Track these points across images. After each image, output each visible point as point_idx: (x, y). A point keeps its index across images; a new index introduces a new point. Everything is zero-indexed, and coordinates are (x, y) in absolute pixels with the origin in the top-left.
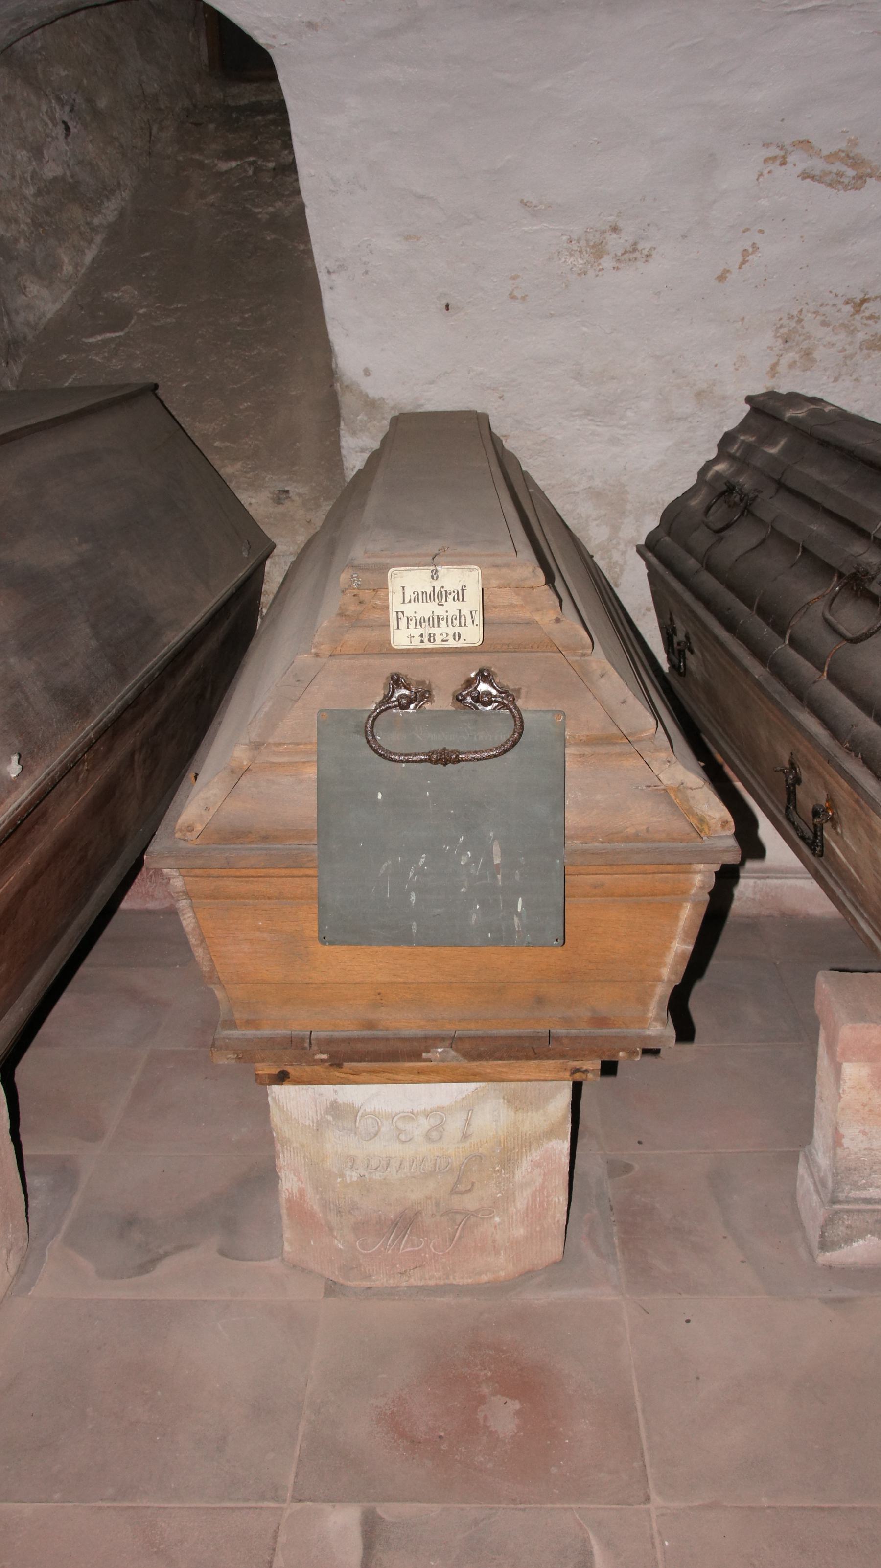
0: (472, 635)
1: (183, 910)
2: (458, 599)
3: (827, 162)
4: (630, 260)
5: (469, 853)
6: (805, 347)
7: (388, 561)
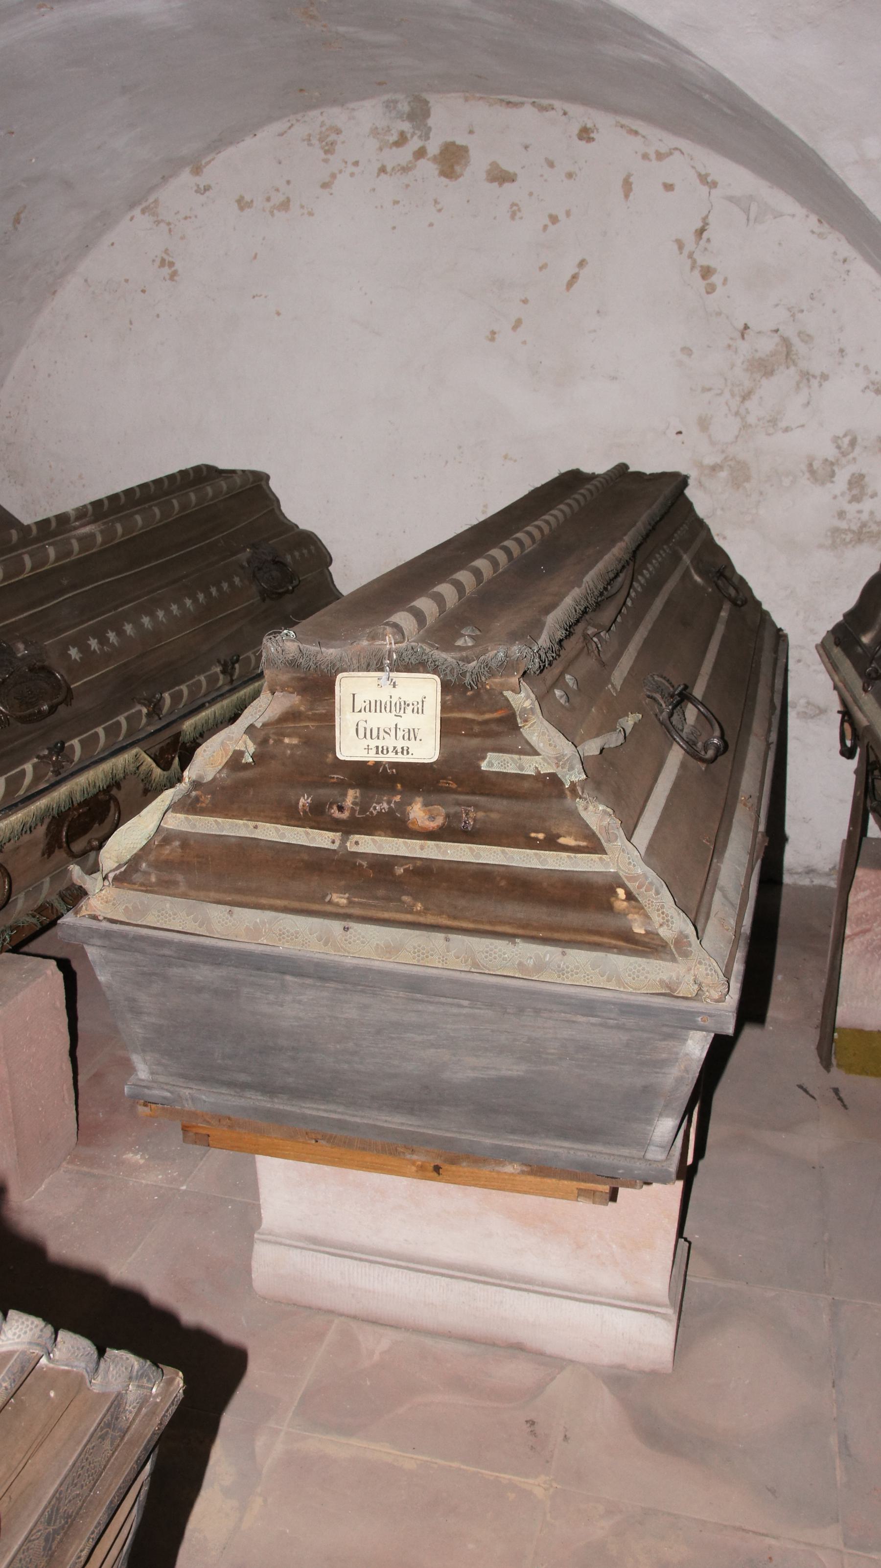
7: (331, 653)
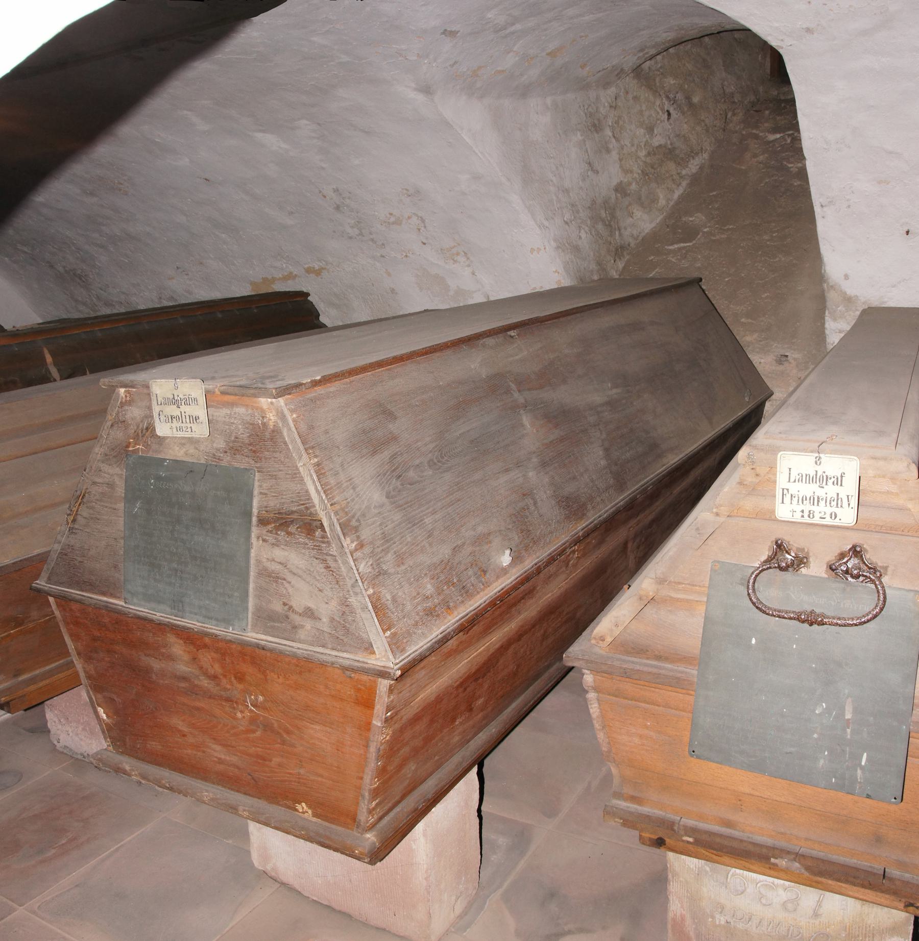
0: (847, 516)
1: (591, 700)
2: (837, 484)
5: (824, 704)
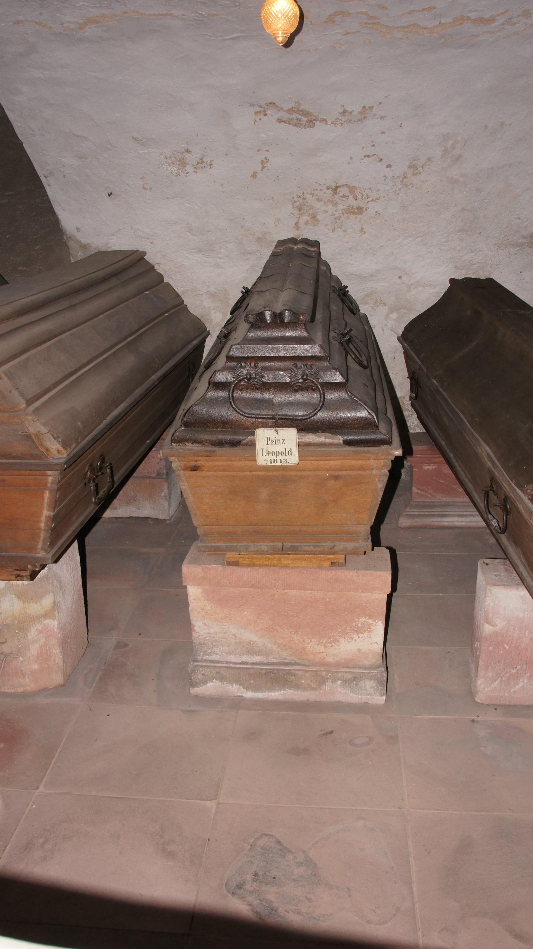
3: (289, 114)
4: (202, 168)
6: (311, 213)
